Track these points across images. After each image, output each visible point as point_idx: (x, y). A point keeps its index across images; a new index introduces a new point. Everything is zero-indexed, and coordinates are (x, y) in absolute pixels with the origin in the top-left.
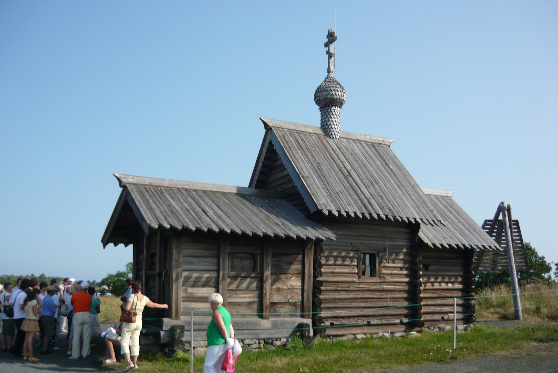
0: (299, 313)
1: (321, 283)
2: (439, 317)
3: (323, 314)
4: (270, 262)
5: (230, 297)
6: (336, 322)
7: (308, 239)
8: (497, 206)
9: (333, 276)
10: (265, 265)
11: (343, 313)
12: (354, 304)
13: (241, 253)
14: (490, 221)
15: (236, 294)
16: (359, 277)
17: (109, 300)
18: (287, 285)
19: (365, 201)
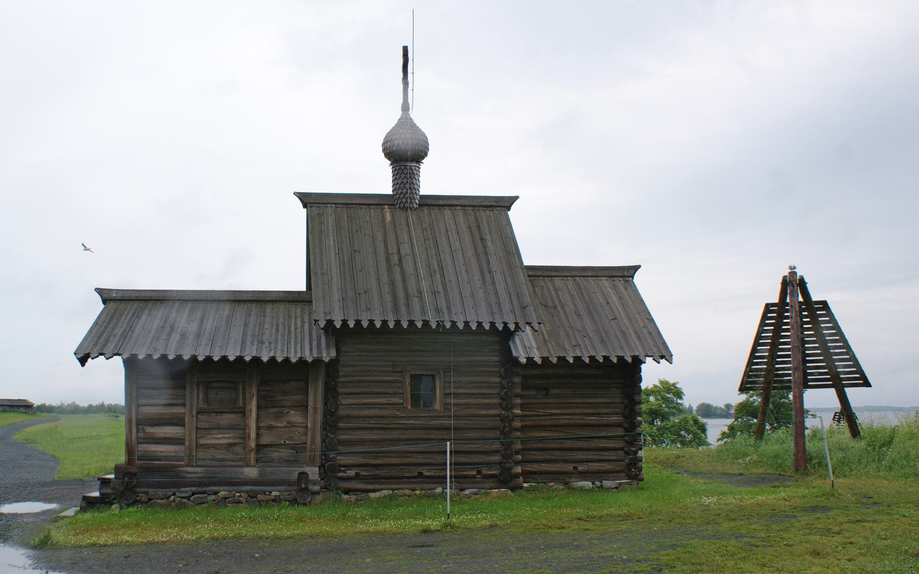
3: (343, 460)
4: (254, 391)
5: (203, 437)
8: (780, 281)
10: (247, 396)
12: (353, 449)
13: (218, 381)
14: (773, 305)
15: (210, 434)
19: (401, 294)
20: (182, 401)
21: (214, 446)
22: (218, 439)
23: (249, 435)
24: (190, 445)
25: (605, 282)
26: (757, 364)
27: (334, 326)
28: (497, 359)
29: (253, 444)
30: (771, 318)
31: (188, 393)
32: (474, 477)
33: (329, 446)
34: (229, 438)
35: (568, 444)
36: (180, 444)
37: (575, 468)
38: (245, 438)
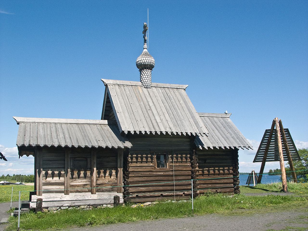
4: (95, 161)
10: (92, 164)
13: (79, 157)
20: (63, 166)
21: (78, 186)
22: (79, 182)
23: (93, 180)
24: (67, 186)
25: (88, 126)
26: (261, 152)
27: (125, 133)
28: (189, 148)
29: (94, 184)
30: (268, 135)
31: (66, 162)
32: (182, 195)
33: (126, 184)
34: (84, 182)
35: (214, 181)
36: (62, 185)
37: (216, 191)
38: (92, 181)
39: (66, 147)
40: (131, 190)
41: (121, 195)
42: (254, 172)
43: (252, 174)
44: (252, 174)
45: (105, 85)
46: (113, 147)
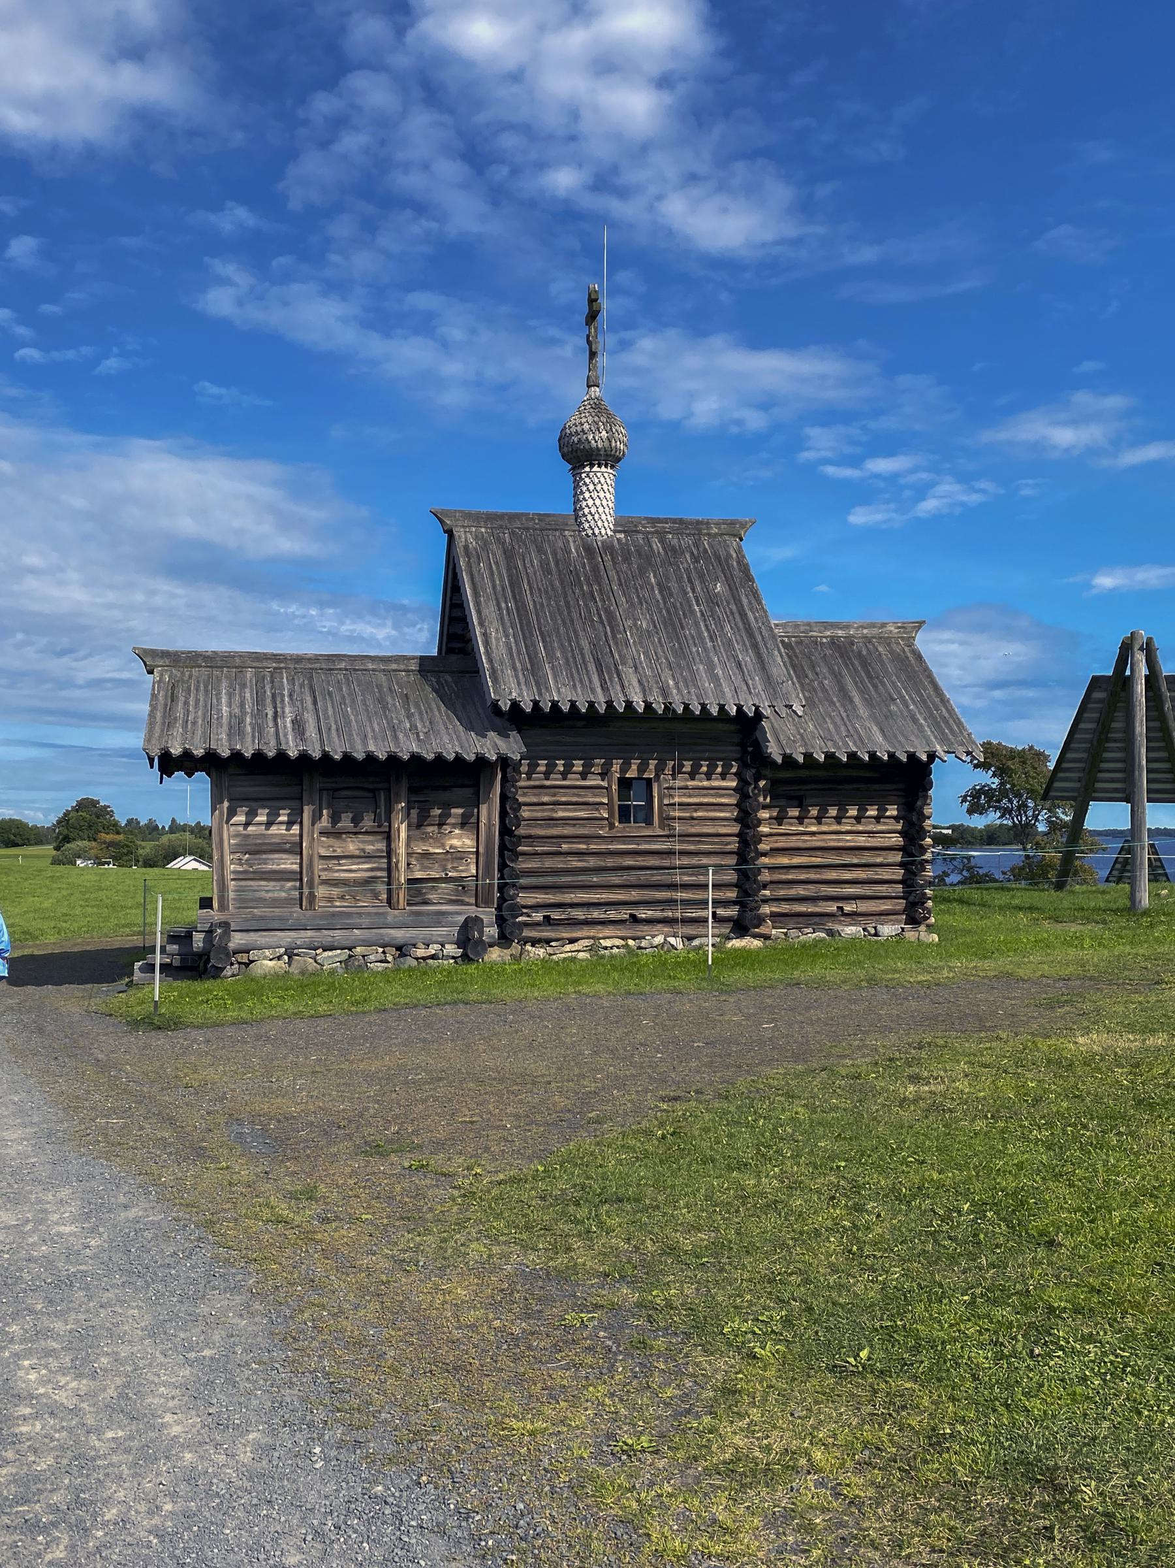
0: (473, 901)
1: (1124, 781)
2: (832, 907)
6: (556, 915)
7: (481, 760)
9: (549, 826)
11: (569, 897)
16: (612, 826)
17: (789, 729)
18: (443, 846)
27: (522, 710)
39: (304, 757)
40: (524, 898)
41: (487, 915)
42: (1140, 657)
43: (1120, 683)
44: (1120, 683)
45: (445, 532)
46: (347, 757)
